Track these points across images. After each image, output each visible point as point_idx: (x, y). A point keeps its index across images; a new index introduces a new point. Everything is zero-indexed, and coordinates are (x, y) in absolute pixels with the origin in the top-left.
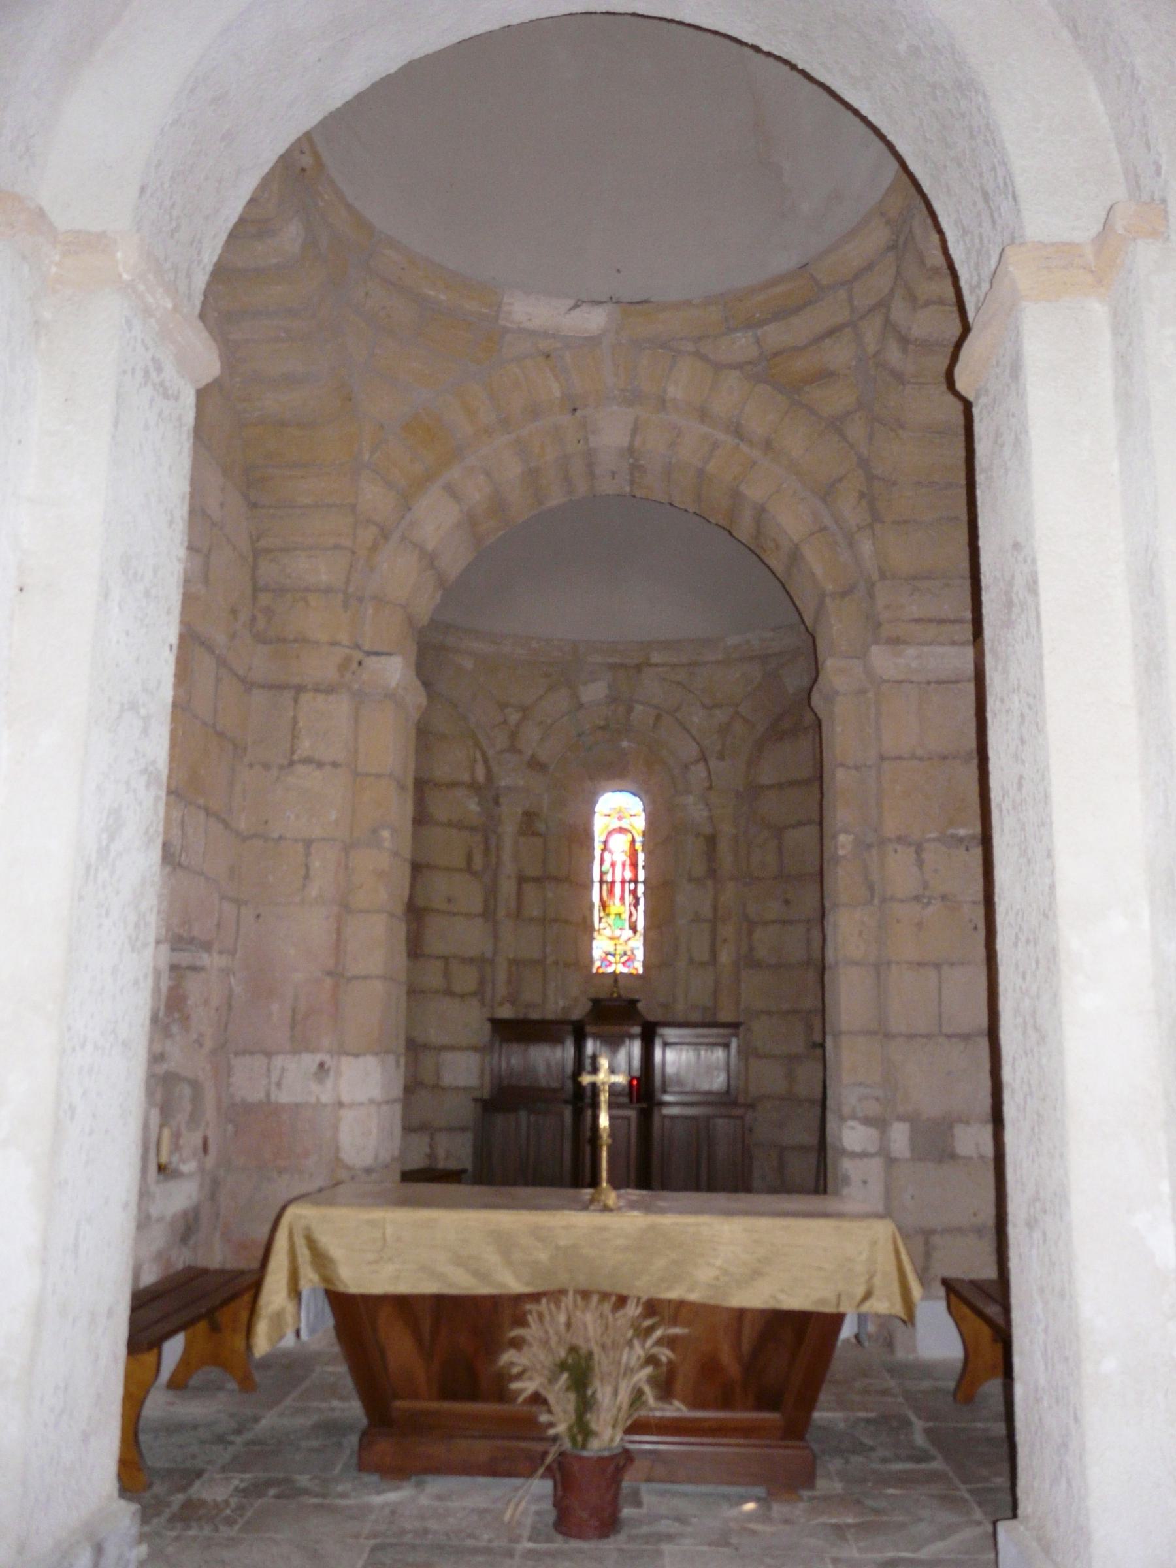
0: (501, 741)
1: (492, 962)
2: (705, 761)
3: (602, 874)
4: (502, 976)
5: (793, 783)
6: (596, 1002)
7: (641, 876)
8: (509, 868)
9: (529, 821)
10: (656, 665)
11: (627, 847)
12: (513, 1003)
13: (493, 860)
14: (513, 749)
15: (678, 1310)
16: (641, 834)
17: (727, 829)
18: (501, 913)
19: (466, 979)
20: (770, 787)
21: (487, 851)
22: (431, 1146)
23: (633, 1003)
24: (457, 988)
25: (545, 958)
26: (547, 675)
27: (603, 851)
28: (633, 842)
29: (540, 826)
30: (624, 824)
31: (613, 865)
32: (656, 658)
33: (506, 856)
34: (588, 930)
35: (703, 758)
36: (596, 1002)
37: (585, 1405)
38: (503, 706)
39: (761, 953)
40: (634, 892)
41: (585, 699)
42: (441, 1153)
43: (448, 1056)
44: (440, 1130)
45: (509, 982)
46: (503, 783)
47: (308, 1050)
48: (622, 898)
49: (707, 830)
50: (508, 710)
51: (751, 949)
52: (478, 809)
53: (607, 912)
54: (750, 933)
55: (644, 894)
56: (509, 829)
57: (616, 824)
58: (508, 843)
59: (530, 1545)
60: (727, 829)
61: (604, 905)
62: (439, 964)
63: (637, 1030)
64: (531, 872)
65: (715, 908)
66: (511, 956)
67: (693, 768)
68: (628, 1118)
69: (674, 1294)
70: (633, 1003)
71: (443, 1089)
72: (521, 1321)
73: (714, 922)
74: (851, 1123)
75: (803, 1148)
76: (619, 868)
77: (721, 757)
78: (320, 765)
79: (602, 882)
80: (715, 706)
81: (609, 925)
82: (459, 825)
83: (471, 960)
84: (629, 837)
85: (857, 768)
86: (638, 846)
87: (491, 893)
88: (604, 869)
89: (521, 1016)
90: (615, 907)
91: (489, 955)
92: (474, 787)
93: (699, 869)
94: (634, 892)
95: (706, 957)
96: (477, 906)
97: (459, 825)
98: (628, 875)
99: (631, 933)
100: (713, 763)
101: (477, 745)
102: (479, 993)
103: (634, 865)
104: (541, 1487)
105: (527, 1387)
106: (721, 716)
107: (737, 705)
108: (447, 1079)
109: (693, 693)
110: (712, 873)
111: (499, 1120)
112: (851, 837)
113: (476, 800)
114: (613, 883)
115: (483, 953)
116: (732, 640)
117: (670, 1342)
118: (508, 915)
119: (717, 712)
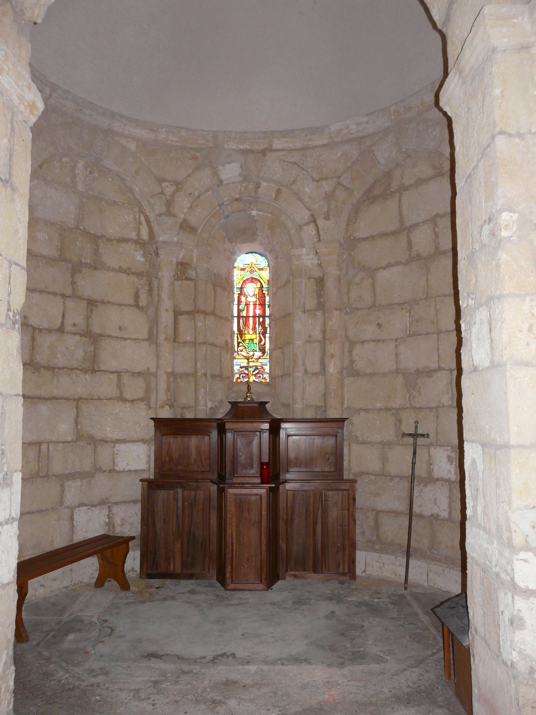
0: (160, 207)
1: (155, 375)
2: (315, 222)
3: (239, 311)
4: (163, 386)
5: (383, 235)
6: (234, 404)
8: (166, 303)
10: (277, 150)
12: (171, 406)
13: (156, 298)
14: (169, 213)
16: (267, 282)
17: (333, 271)
18: (162, 337)
20: (365, 239)
21: (150, 291)
22: (109, 517)
23: (263, 404)
24: (128, 395)
25: (196, 372)
26: (195, 158)
27: (240, 295)
28: (262, 287)
29: (191, 273)
30: (255, 275)
31: (247, 305)
32: (277, 144)
33: (165, 296)
35: (314, 220)
36: (234, 404)
38: (160, 181)
39: (360, 365)
40: (263, 324)
41: (223, 177)
42: (117, 521)
43: (121, 447)
44: (116, 503)
45: (168, 390)
46: (161, 239)
48: (254, 328)
49: (317, 274)
50: (165, 184)
51: (352, 362)
52: (143, 259)
53: (243, 338)
54: (350, 351)
55: (269, 325)
57: (248, 275)
58: (166, 285)
60: (333, 271)
61: (241, 333)
62: (114, 377)
63: (266, 426)
64: (185, 308)
65: (324, 332)
66: (169, 370)
67: (305, 228)
68: (261, 496)
70: (263, 404)
71: (118, 472)
73: (324, 342)
74: (522, 555)
75: (396, 513)
76: (251, 307)
77: (327, 218)
79: (239, 317)
80: (322, 179)
81: (245, 348)
82: (128, 272)
83: (139, 374)
84: (259, 285)
85: (521, 136)
88: (240, 308)
89: (179, 417)
91: (153, 370)
92: (139, 242)
93: (311, 303)
95: (317, 368)
97: (128, 272)
99: (260, 354)
100: (321, 222)
101: (141, 211)
102: (145, 399)
106: (327, 186)
107: (339, 177)
108: (121, 465)
109: (306, 170)
110: (321, 306)
111: (162, 494)
112: (515, 216)
113: (142, 252)
114: (247, 317)
115: (149, 368)
116: (334, 128)
118: (166, 339)
119: (324, 183)
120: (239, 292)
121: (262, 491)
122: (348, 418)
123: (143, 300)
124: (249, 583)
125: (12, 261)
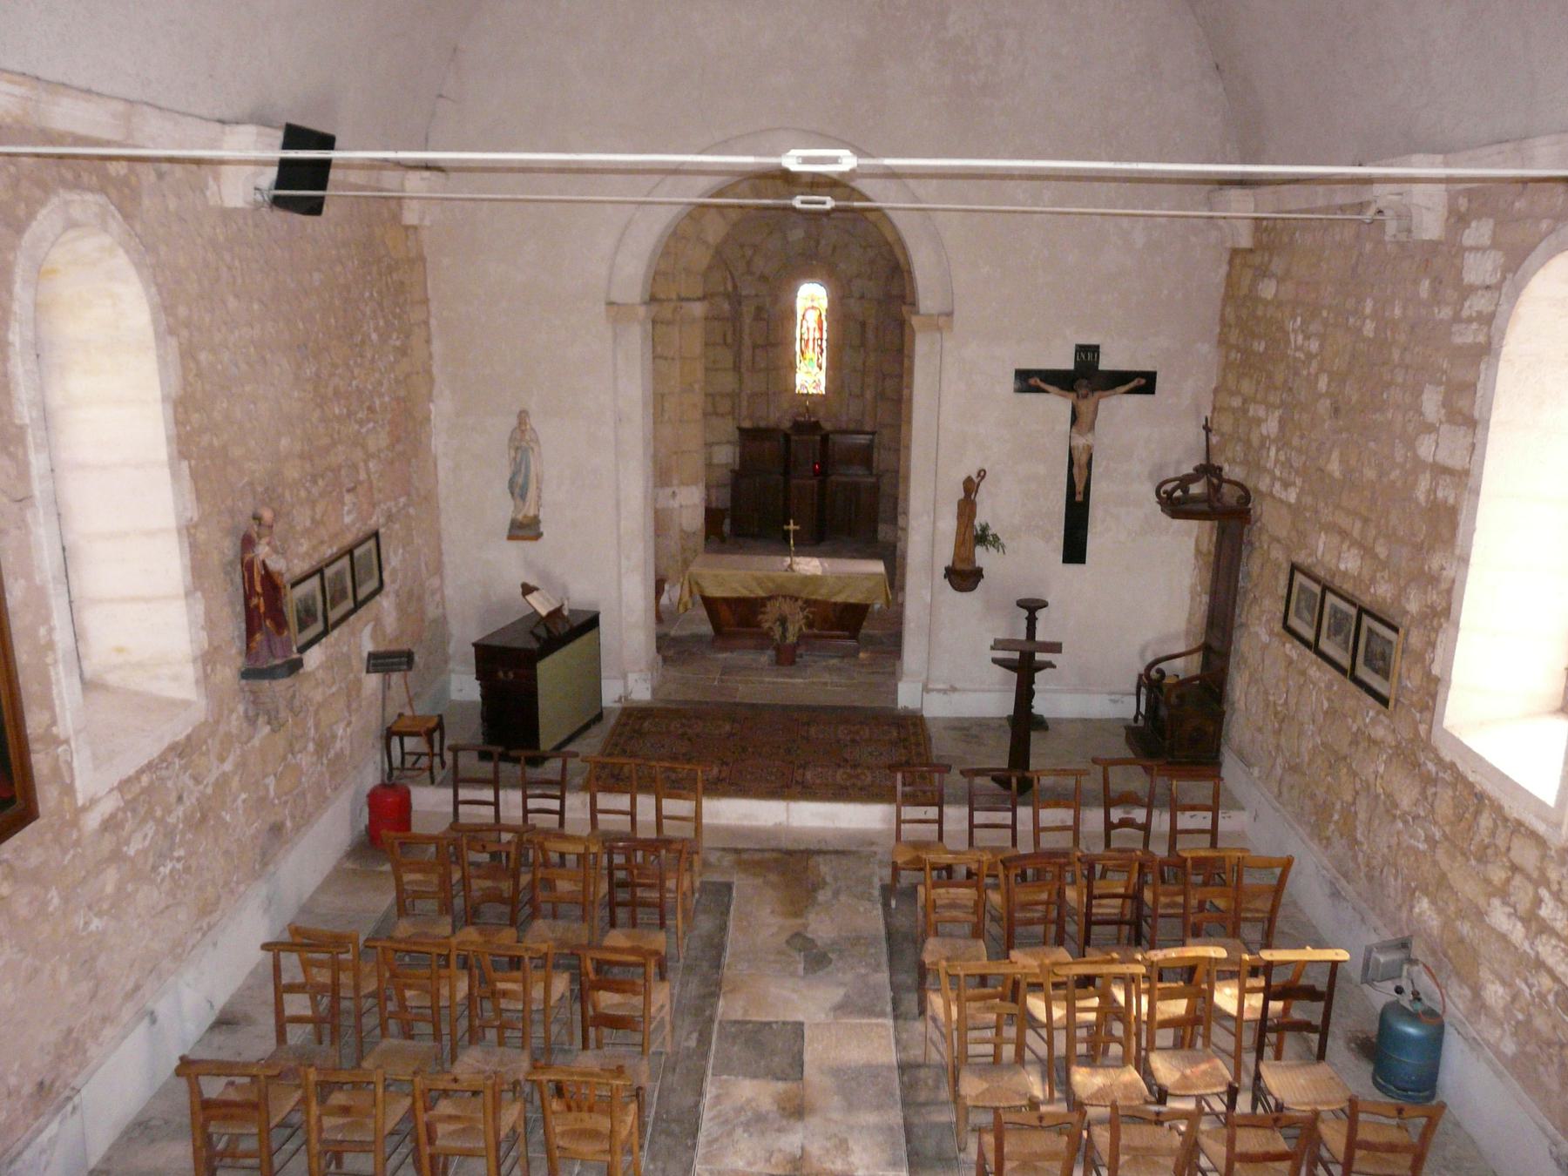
7: (825, 336)
8: (747, 341)
9: (759, 313)
11: (816, 318)
15: (816, 602)
17: (872, 322)
19: (725, 406)
30: (815, 304)
34: (793, 368)
37: (785, 630)
38: (742, 246)
40: (821, 346)
47: (667, 485)
49: (861, 319)
56: (747, 321)
57: (809, 304)
59: (680, 917)
60: (872, 322)
63: (818, 438)
69: (814, 597)
72: (765, 606)
78: (666, 359)
83: (728, 394)
86: (823, 318)
87: (738, 355)
90: (809, 354)
92: (727, 296)
94: (821, 346)
96: (729, 364)
98: (817, 335)
102: (732, 412)
103: (821, 329)
104: (771, 653)
105: (766, 625)
106: (871, 253)
110: (863, 344)
117: (813, 613)
120: (888, 880)
121: (815, 482)
122: (523, 416)
123: (729, 340)
124: (759, 850)
125: (990, 532)
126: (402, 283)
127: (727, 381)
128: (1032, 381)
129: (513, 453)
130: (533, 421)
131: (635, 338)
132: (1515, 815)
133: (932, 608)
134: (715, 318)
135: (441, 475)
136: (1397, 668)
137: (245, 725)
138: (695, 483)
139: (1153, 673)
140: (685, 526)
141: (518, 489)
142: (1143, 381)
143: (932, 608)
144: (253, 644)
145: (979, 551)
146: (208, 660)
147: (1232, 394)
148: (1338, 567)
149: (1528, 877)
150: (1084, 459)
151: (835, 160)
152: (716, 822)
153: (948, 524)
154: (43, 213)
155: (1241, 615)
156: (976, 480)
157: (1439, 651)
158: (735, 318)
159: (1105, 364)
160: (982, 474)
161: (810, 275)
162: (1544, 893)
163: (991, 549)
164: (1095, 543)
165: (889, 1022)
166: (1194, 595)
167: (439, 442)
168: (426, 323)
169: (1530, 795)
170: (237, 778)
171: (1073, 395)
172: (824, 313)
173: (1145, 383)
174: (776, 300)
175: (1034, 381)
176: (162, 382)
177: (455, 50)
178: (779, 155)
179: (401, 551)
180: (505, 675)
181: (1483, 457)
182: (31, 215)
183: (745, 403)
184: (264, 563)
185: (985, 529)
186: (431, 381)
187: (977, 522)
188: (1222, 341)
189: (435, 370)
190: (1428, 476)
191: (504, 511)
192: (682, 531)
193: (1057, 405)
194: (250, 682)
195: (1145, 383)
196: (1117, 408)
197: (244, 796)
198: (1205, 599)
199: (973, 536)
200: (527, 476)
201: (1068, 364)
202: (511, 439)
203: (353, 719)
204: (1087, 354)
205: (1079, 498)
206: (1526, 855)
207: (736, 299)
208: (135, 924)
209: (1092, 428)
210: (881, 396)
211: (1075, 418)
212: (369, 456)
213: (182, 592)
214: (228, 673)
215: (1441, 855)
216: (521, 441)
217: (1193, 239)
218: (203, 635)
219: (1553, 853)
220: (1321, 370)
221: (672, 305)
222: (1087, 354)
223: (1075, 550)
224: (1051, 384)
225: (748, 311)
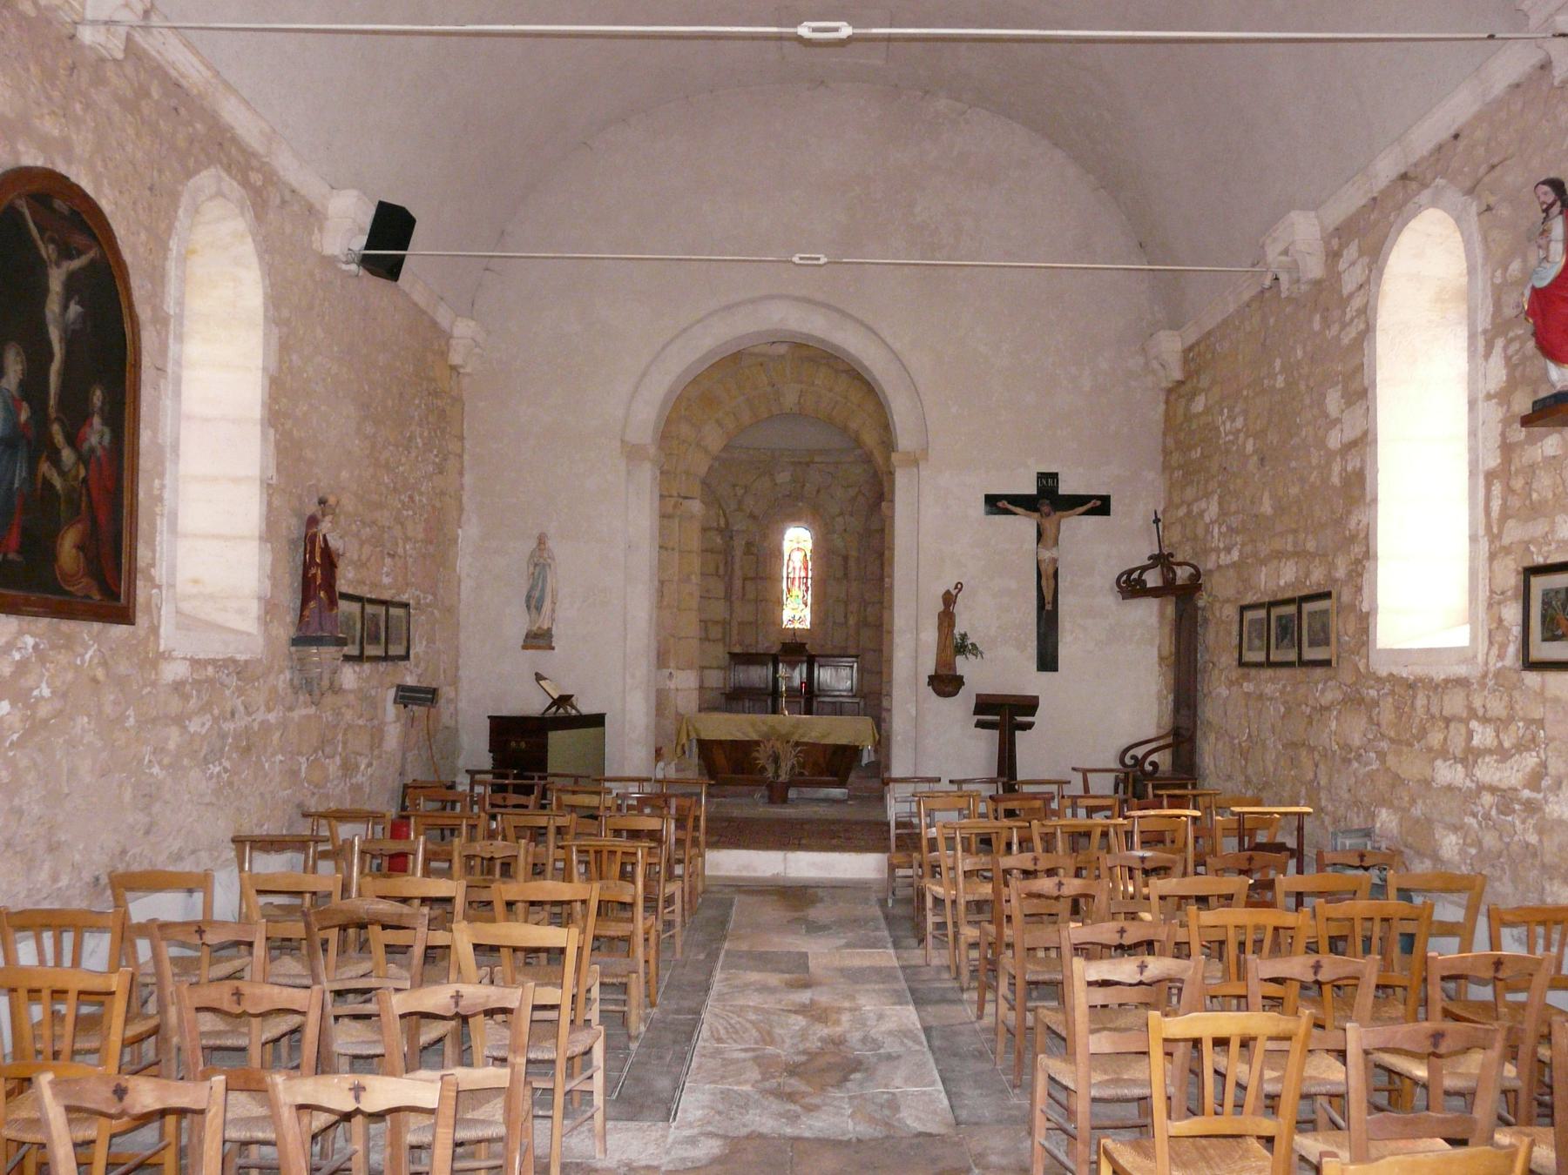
8: (738, 573)
19: (716, 632)
34: (780, 604)
37: (778, 768)
56: (738, 553)
90: (796, 591)
92: (719, 530)
96: (722, 594)
98: (803, 574)
102: (723, 639)
103: (806, 569)
104: (764, 790)
106: (852, 492)
126: (444, 411)
127: (718, 610)
128: (1000, 504)
129: (531, 569)
130: (550, 544)
131: (646, 475)
132: (1442, 677)
133: (917, 721)
134: (706, 551)
135: (463, 595)
136: (1335, 630)
137: (289, 691)
138: (690, 667)
139: (1128, 761)
140: (681, 711)
141: (534, 603)
142: (1099, 503)
143: (917, 721)
144: (306, 613)
145: (960, 660)
146: (270, 608)
147: (1178, 507)
148: (1278, 585)
149: (1461, 720)
150: (1051, 571)
151: (836, 30)
152: (714, 873)
153: (930, 636)
154: (204, 173)
155: (1203, 688)
156: (954, 592)
157: (1366, 591)
158: (727, 552)
159: (1064, 489)
160: (959, 587)
161: (795, 518)
162: (1474, 724)
163: (971, 657)
164: (1067, 649)
165: (892, 951)
166: (1160, 698)
167: (464, 563)
168: (461, 456)
169: (1451, 649)
170: (278, 734)
171: (1036, 515)
172: (809, 554)
173: (1101, 506)
174: (764, 536)
175: (1003, 504)
176: (264, 354)
177: (503, 233)
178: (795, 26)
179: (424, 643)
180: (518, 745)
181: (1375, 398)
182: (197, 172)
183: (735, 631)
184: (324, 536)
185: (964, 636)
186: (461, 509)
187: (956, 631)
188: (1166, 467)
189: (465, 499)
190: (1338, 459)
191: (517, 624)
192: (677, 714)
193: (1023, 526)
194: (300, 648)
195: (1101, 506)
196: (1077, 528)
197: (280, 757)
198: (1171, 697)
199: (955, 645)
200: (543, 590)
201: (1031, 489)
202: (532, 556)
203: (375, 763)
204: (1047, 481)
205: (1049, 607)
206: (1454, 703)
207: (727, 532)
208: (186, 797)
209: (1056, 542)
210: (863, 623)
211: (1040, 535)
212: (407, 539)
213: (257, 534)
214: (284, 630)
215: (1391, 761)
216: (540, 563)
217: (1133, 383)
218: (268, 583)
219: (1475, 686)
220: (1247, 437)
221: (673, 501)
222: (1047, 481)
223: (1048, 661)
224: (1020, 506)
225: (739, 544)
